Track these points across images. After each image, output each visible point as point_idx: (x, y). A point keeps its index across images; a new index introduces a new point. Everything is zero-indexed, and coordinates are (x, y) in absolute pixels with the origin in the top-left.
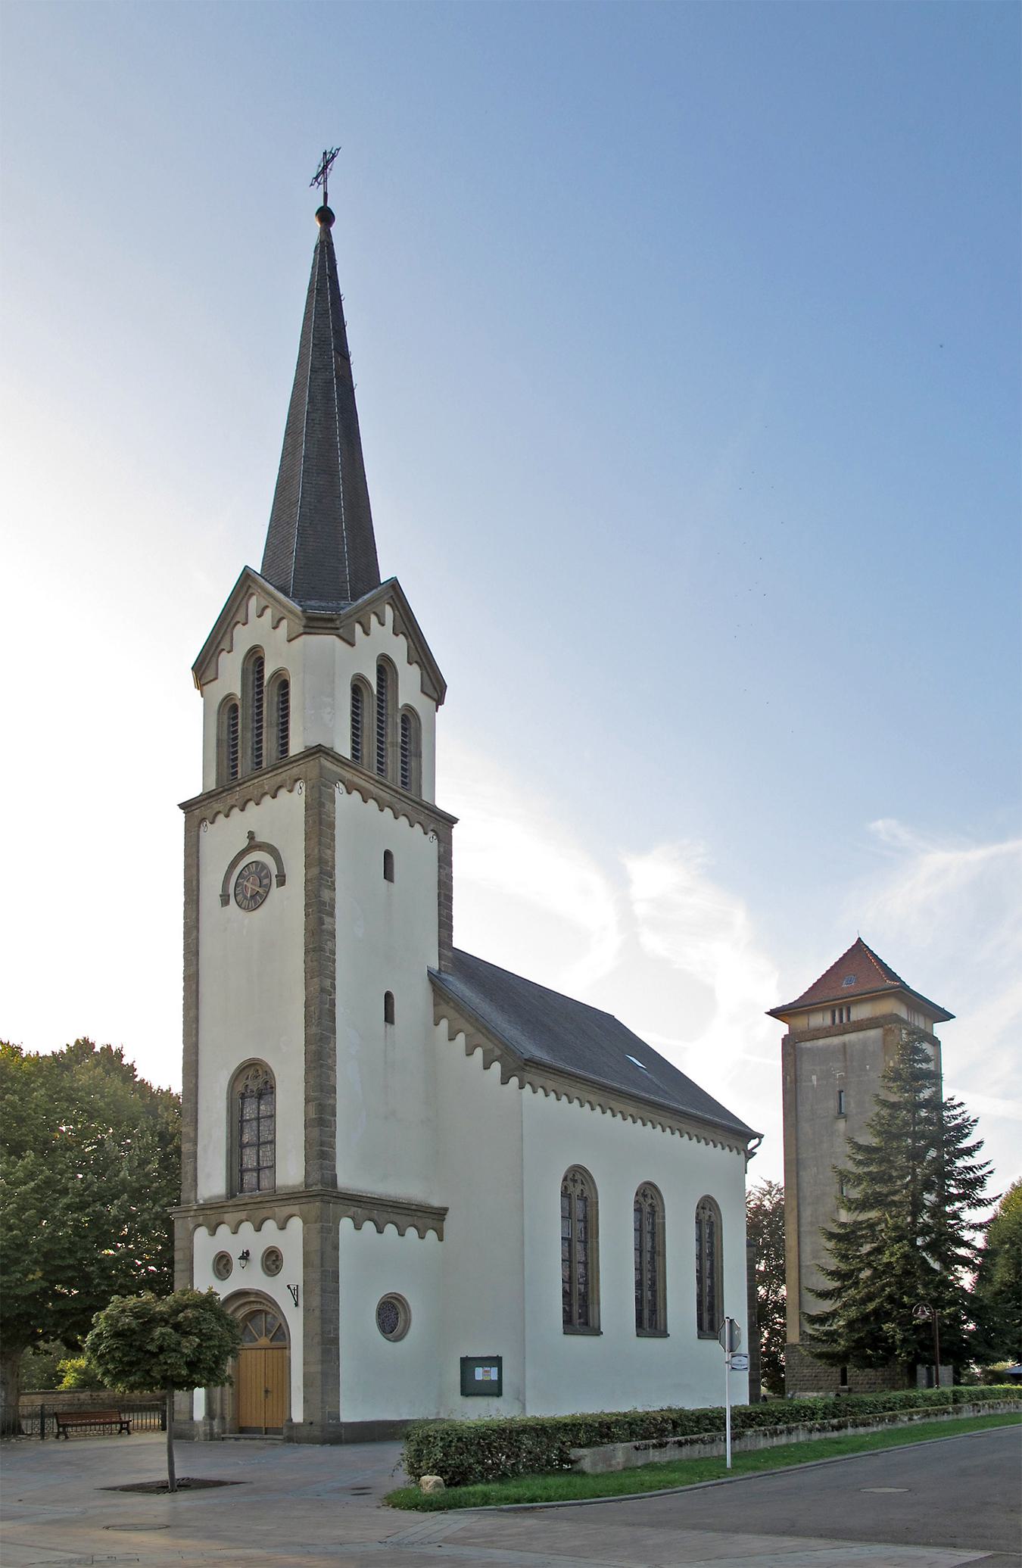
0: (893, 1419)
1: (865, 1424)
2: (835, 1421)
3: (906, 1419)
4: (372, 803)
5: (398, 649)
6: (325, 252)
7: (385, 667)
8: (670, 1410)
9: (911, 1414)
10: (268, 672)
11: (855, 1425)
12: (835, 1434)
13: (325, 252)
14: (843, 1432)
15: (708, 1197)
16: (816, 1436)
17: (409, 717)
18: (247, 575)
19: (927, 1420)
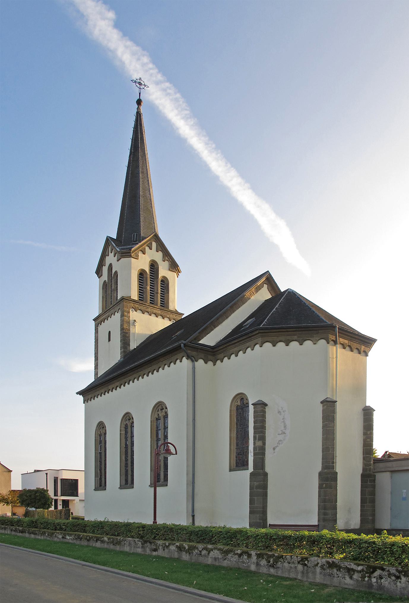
0: (51, 535)
1: (35, 534)
2: (21, 528)
3: (60, 537)
4: (159, 317)
5: (158, 256)
6: (139, 115)
7: (154, 266)
8: (174, 525)
9: (65, 535)
10: (113, 272)
11: (30, 533)
12: (21, 534)
13: (139, 115)
14: (23, 535)
15: (102, 422)
16: (13, 533)
17: (165, 282)
18: (108, 240)
19: (78, 542)
